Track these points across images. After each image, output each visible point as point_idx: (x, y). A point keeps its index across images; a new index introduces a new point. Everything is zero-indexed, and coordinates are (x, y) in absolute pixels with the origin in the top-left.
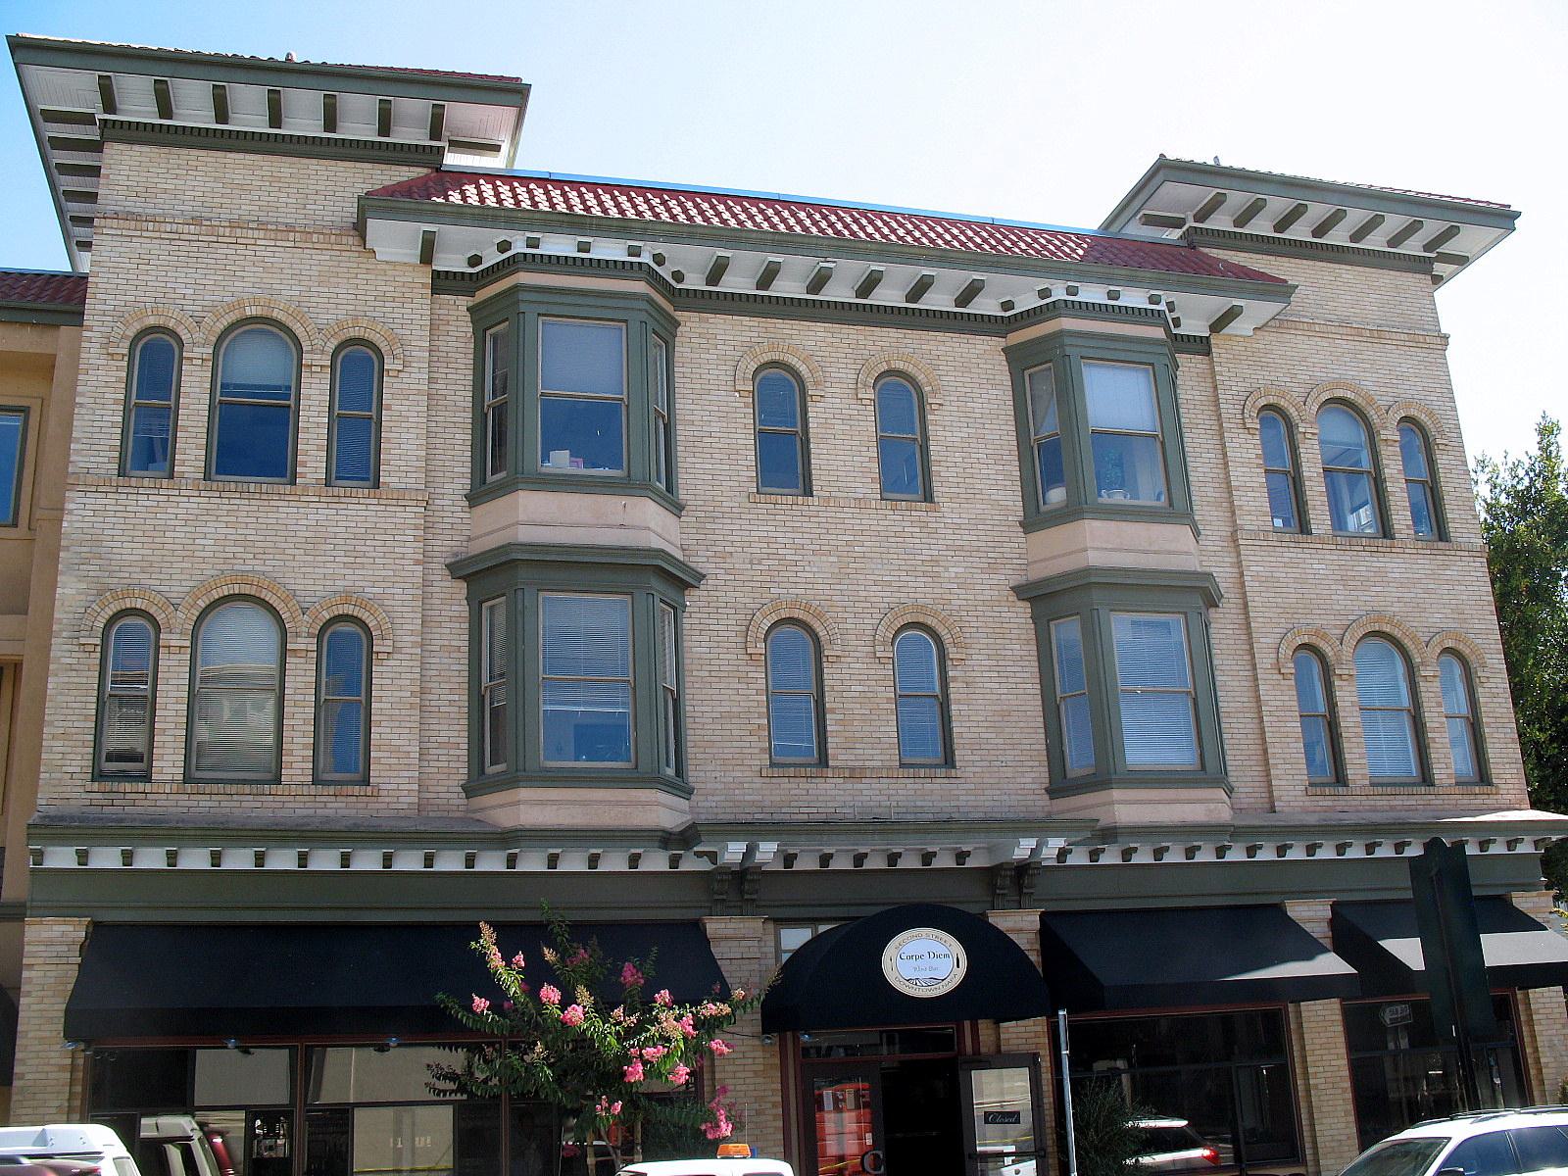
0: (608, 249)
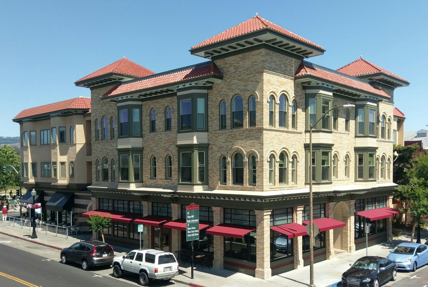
0: (125, 98)
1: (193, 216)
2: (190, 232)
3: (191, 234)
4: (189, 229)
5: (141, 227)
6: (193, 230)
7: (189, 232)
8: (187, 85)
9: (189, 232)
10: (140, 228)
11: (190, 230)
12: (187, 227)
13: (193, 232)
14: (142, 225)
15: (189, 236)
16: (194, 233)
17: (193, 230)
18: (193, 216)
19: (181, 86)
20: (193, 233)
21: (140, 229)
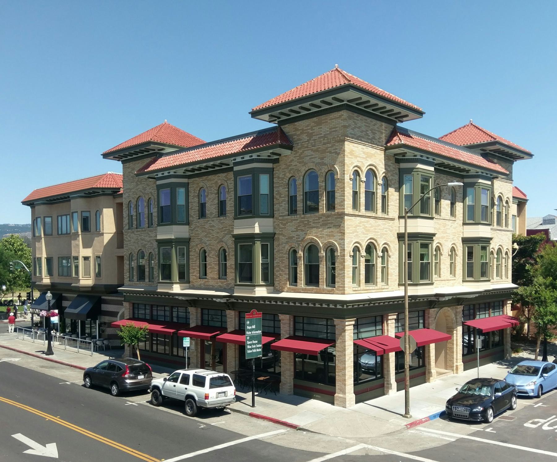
1: (254, 327)
2: (250, 347)
3: (251, 349)
4: (249, 343)
5: (187, 340)
6: (254, 344)
7: (249, 347)
8: (247, 157)
9: (249, 347)
10: (186, 342)
11: (250, 345)
12: (247, 340)
13: (254, 346)
14: (189, 338)
15: (249, 352)
16: (256, 348)
17: (254, 344)
18: (254, 327)
19: (239, 159)
20: (254, 348)
21: (186, 343)
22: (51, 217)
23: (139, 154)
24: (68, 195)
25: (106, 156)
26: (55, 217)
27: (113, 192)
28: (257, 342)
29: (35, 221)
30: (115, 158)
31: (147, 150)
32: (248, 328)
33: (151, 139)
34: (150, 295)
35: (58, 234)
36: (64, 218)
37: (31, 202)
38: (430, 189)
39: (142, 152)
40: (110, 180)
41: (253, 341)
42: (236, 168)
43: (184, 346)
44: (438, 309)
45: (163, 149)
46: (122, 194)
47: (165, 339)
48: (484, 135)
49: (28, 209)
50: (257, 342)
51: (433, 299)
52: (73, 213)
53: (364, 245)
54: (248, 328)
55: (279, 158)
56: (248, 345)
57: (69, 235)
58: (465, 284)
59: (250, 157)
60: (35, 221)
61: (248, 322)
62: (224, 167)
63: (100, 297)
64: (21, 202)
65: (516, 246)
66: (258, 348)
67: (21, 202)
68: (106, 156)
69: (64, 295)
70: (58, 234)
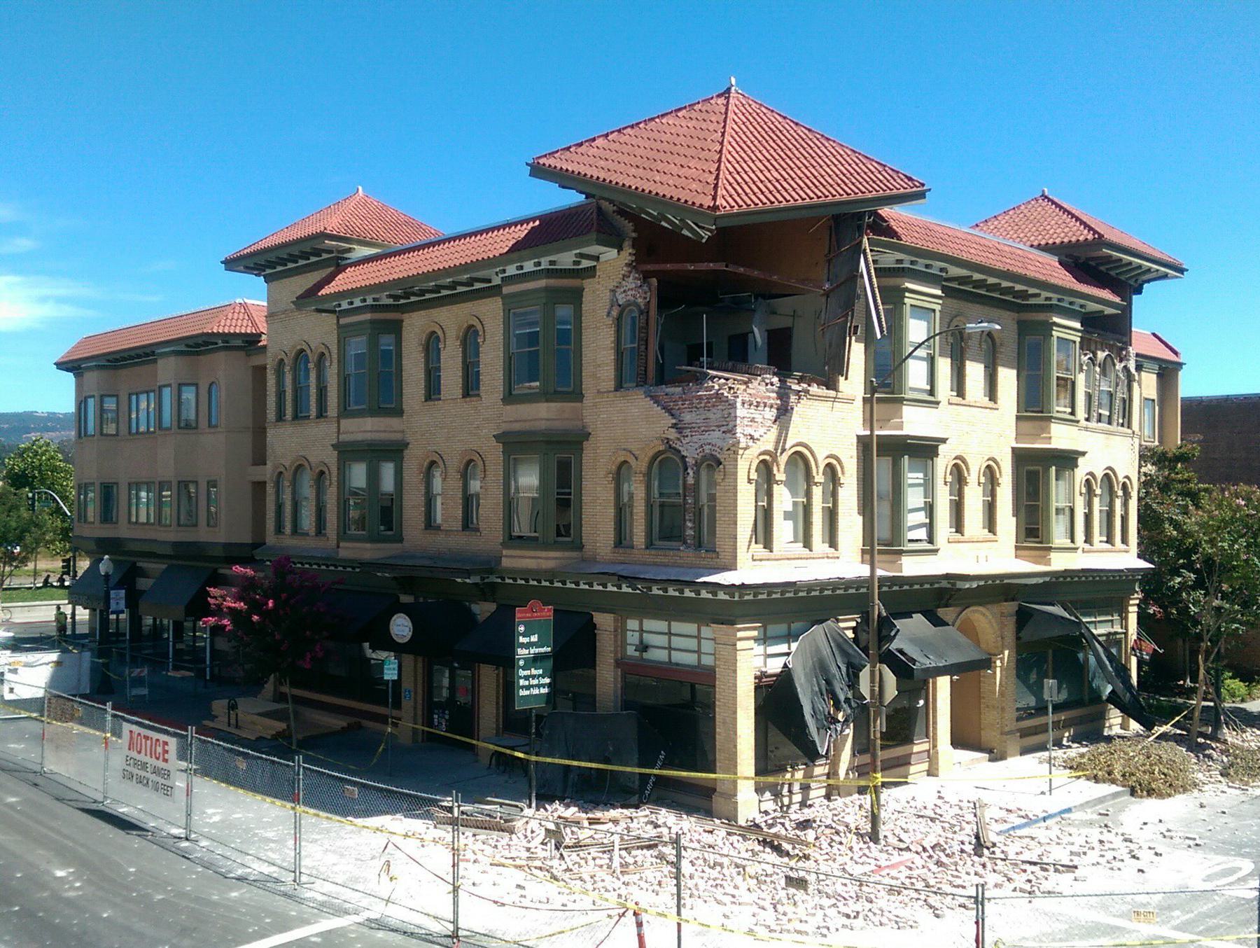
0: (357, 303)
1: (534, 638)
2: (527, 683)
3: (528, 688)
6: (534, 677)
7: (522, 682)
9: (522, 682)
10: (390, 669)
11: (526, 678)
13: (535, 682)
15: (523, 693)
16: (539, 686)
17: (534, 677)
18: (534, 638)
19: (511, 270)
20: (533, 686)
22: (117, 396)
23: (311, 258)
24: (153, 348)
25: (232, 264)
26: (124, 398)
27: (247, 342)
28: (541, 672)
29: (83, 405)
30: (248, 269)
31: (317, 253)
32: (522, 640)
33: (325, 229)
34: (319, 566)
35: (130, 433)
36: (143, 397)
37: (75, 365)
38: (937, 338)
39: (305, 256)
40: (241, 316)
41: (533, 669)
42: (505, 290)
43: (386, 677)
44: (958, 609)
45: (349, 250)
46: (265, 347)
47: (194, 634)
48: (1061, 213)
49: (69, 378)
50: (541, 672)
51: (944, 584)
52: (160, 388)
53: (1099, 475)
54: (522, 640)
55: (595, 267)
56: (521, 678)
57: (153, 435)
58: (1085, 554)
59: (535, 266)
60: (83, 405)
61: (522, 629)
62: (478, 286)
63: (216, 570)
64: (55, 364)
65: (1150, 468)
66: (543, 686)
67: (55, 364)
68: (232, 264)
69: (139, 564)
70: (130, 433)
